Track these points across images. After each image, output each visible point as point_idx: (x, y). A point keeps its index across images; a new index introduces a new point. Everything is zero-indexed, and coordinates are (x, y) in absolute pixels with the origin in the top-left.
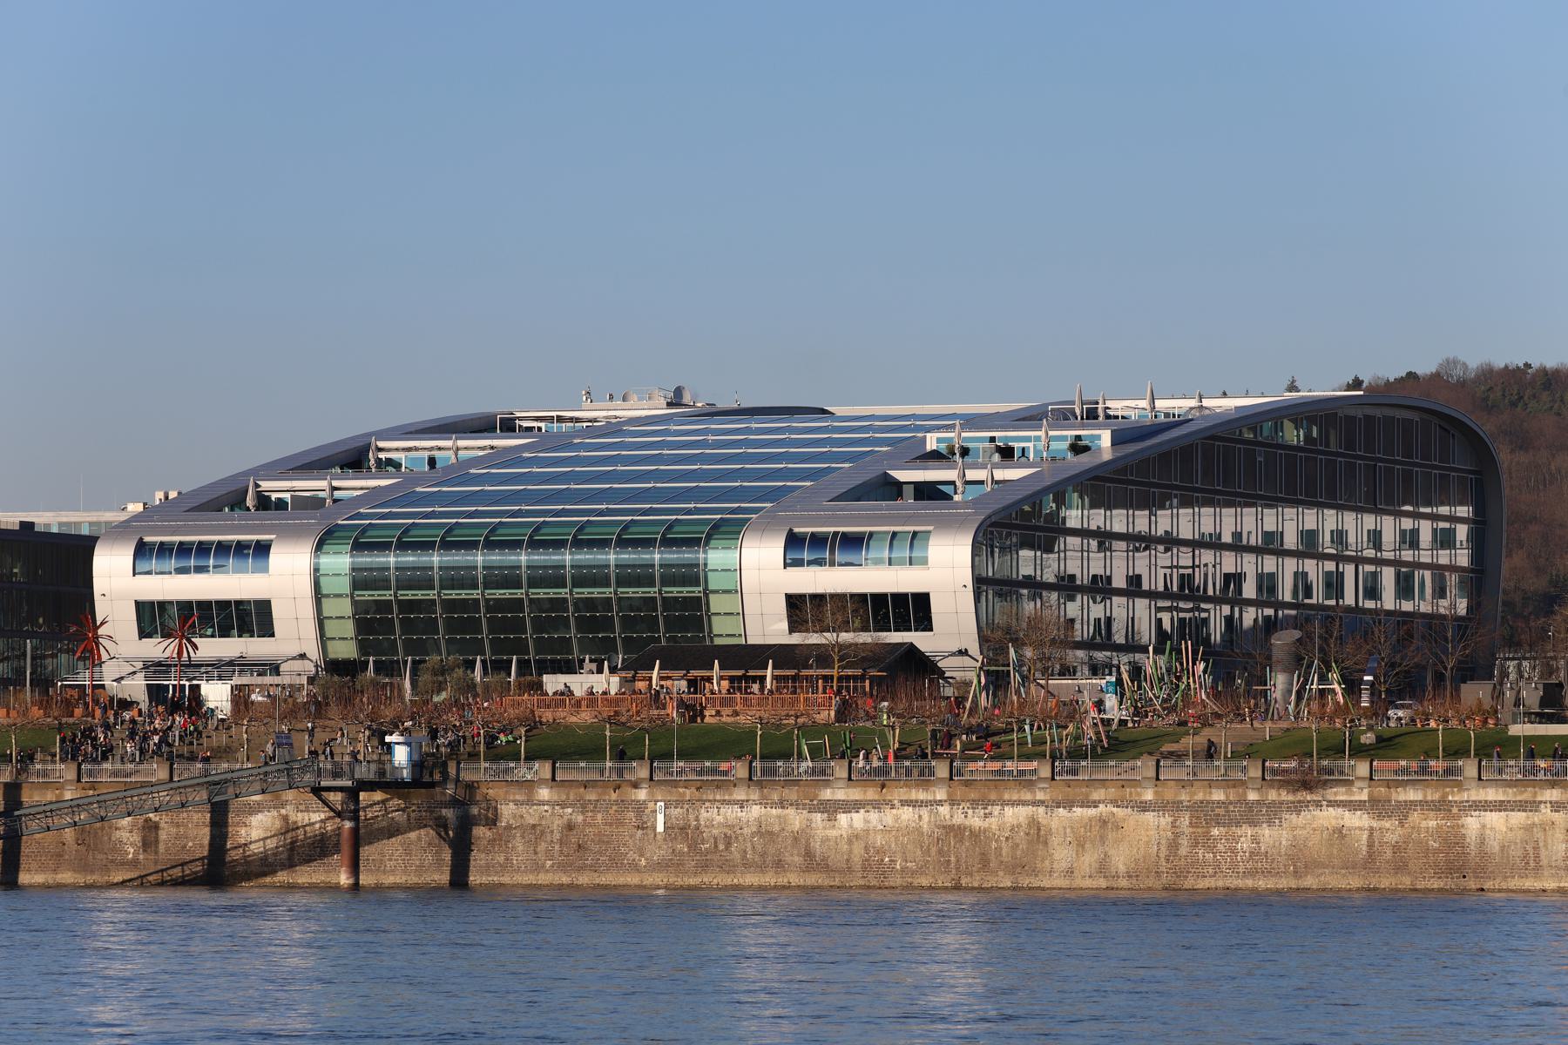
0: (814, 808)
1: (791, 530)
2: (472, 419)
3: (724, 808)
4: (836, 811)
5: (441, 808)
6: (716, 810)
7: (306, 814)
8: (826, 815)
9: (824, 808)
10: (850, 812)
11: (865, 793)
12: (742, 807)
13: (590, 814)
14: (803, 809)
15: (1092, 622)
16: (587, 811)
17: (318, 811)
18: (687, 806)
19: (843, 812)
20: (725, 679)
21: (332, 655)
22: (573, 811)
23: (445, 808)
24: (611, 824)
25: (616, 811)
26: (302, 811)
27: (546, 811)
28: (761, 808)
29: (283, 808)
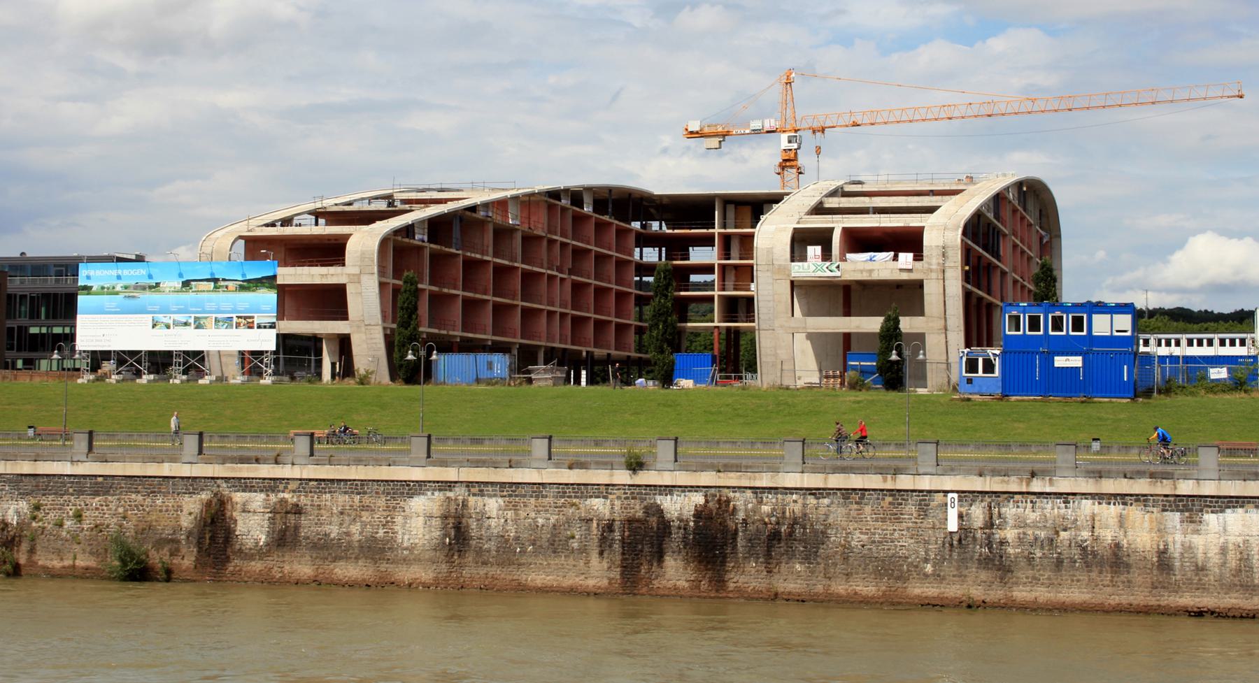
0: (1170, 506)
1: (918, 257)
2: (329, 240)
3: (1042, 502)
4: (1201, 511)
5: (655, 494)
6: (1029, 505)
7: (479, 498)
8: (1187, 514)
9: (1183, 506)
10: (1222, 511)
11: (612, 475)
12: (1066, 502)
13: (855, 506)
14: (1153, 506)
15: (912, 221)
16: (852, 503)
17: (495, 495)
18: (989, 500)
19: (1212, 512)
20: (71, 330)
21: (506, 373)
22: (832, 503)
23: (660, 495)
24: (883, 520)
25: (890, 503)
26: (474, 495)
27: (795, 501)
28: (1094, 504)
29: (451, 490)
